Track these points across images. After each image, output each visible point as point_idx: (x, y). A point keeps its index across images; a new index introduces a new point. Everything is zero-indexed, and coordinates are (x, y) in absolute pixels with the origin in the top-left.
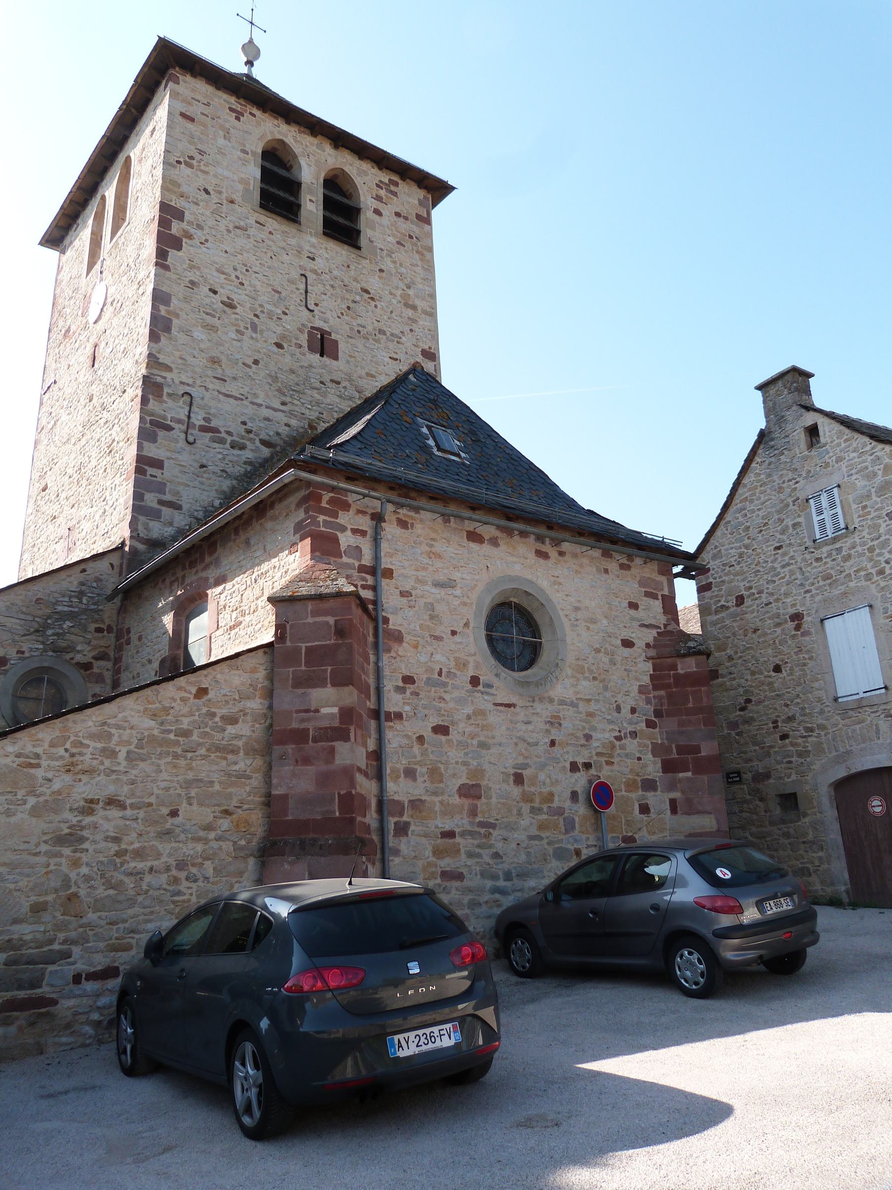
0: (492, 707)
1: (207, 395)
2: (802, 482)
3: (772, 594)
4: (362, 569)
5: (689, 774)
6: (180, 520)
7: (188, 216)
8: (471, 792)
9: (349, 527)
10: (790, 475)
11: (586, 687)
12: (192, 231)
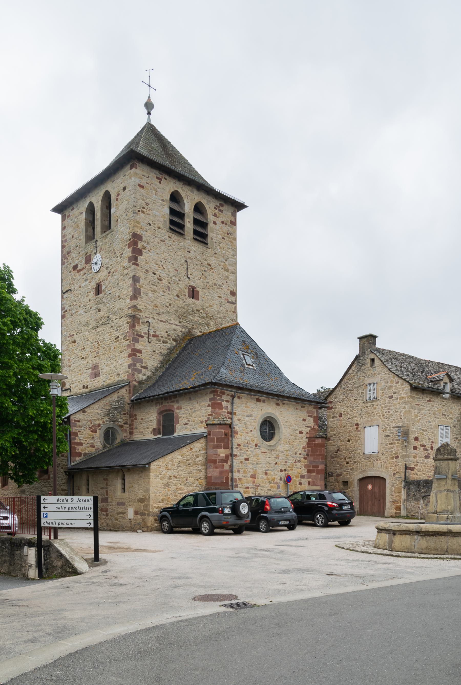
0: (260, 453)
1: (154, 321)
2: (366, 378)
3: (351, 415)
4: (228, 413)
5: (315, 474)
6: (148, 373)
7: (144, 238)
10: (363, 374)
11: (287, 447)
12: (146, 245)
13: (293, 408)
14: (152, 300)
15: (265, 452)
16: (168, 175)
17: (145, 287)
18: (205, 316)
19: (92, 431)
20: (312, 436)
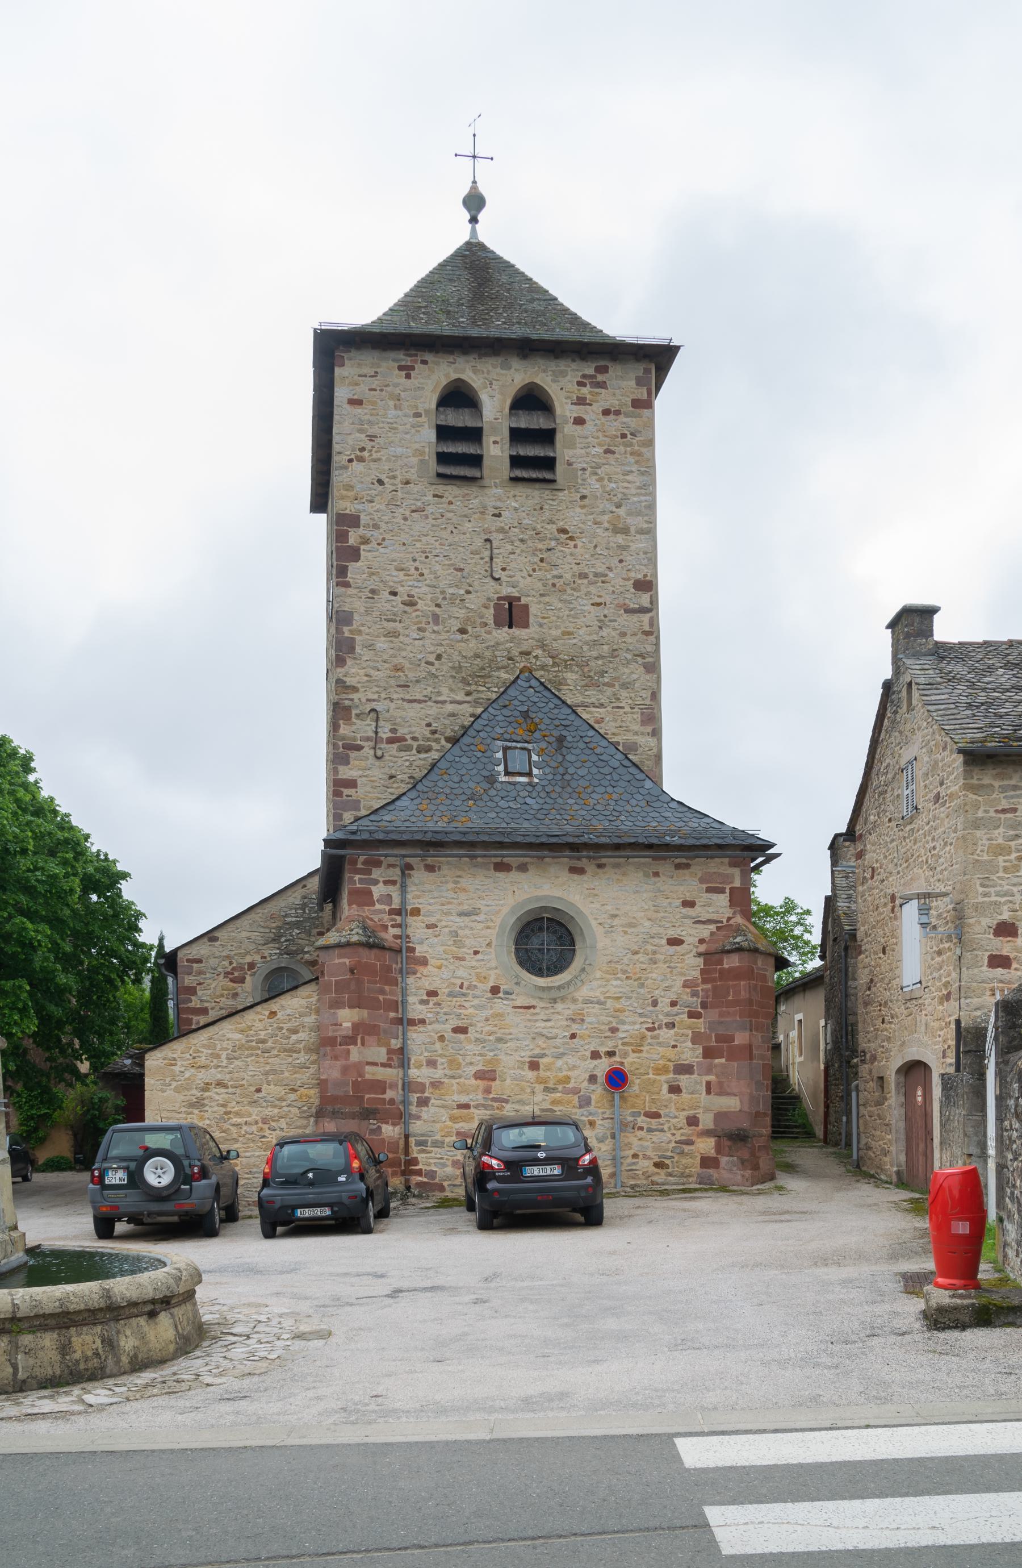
0: (510, 1010)
1: (393, 705)
4: (392, 912)
5: (723, 1060)
7: (364, 519)
8: (487, 1076)
9: (381, 879)
11: (615, 986)
12: (369, 534)
13: (641, 874)
14: (385, 657)
15: (529, 1008)
16: (430, 351)
17: (367, 631)
18: (550, 661)
19: (232, 981)
20: (714, 947)
